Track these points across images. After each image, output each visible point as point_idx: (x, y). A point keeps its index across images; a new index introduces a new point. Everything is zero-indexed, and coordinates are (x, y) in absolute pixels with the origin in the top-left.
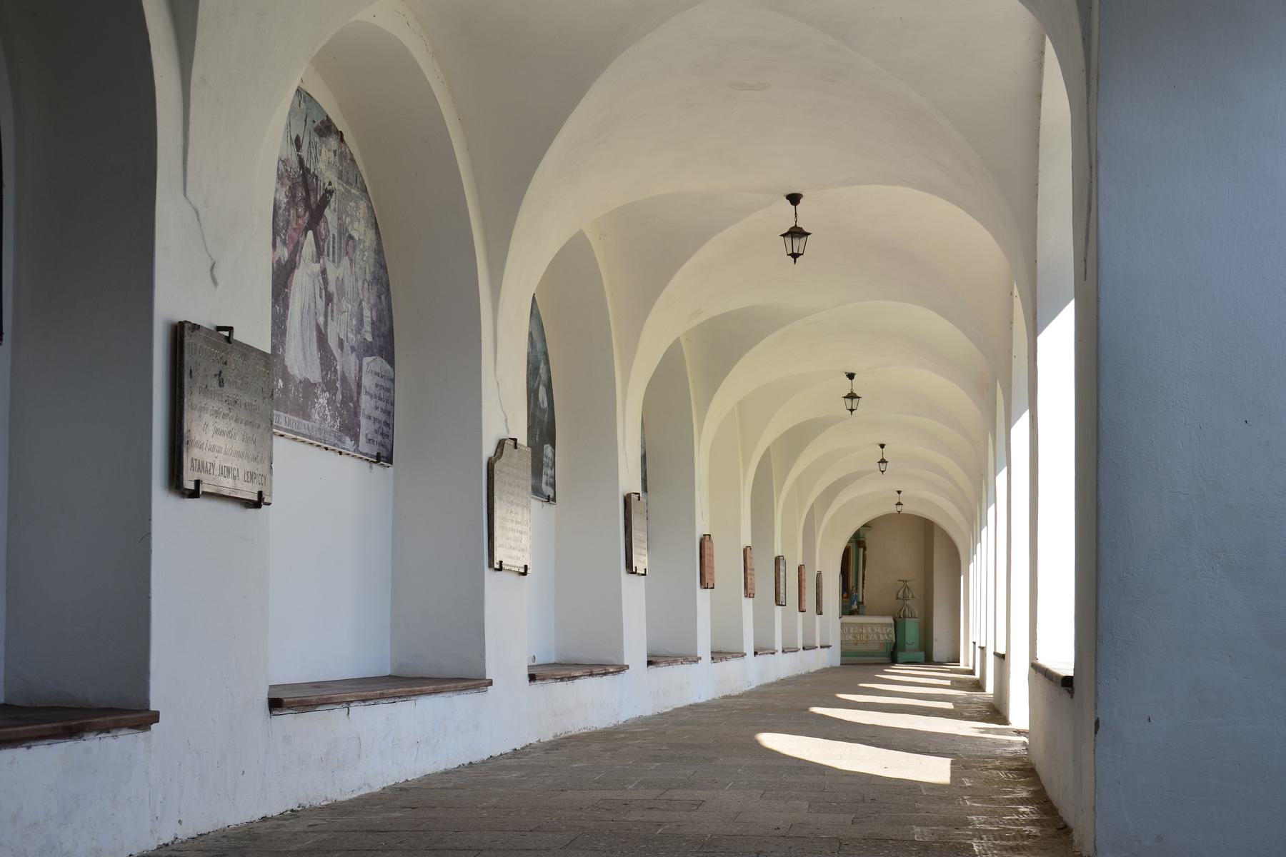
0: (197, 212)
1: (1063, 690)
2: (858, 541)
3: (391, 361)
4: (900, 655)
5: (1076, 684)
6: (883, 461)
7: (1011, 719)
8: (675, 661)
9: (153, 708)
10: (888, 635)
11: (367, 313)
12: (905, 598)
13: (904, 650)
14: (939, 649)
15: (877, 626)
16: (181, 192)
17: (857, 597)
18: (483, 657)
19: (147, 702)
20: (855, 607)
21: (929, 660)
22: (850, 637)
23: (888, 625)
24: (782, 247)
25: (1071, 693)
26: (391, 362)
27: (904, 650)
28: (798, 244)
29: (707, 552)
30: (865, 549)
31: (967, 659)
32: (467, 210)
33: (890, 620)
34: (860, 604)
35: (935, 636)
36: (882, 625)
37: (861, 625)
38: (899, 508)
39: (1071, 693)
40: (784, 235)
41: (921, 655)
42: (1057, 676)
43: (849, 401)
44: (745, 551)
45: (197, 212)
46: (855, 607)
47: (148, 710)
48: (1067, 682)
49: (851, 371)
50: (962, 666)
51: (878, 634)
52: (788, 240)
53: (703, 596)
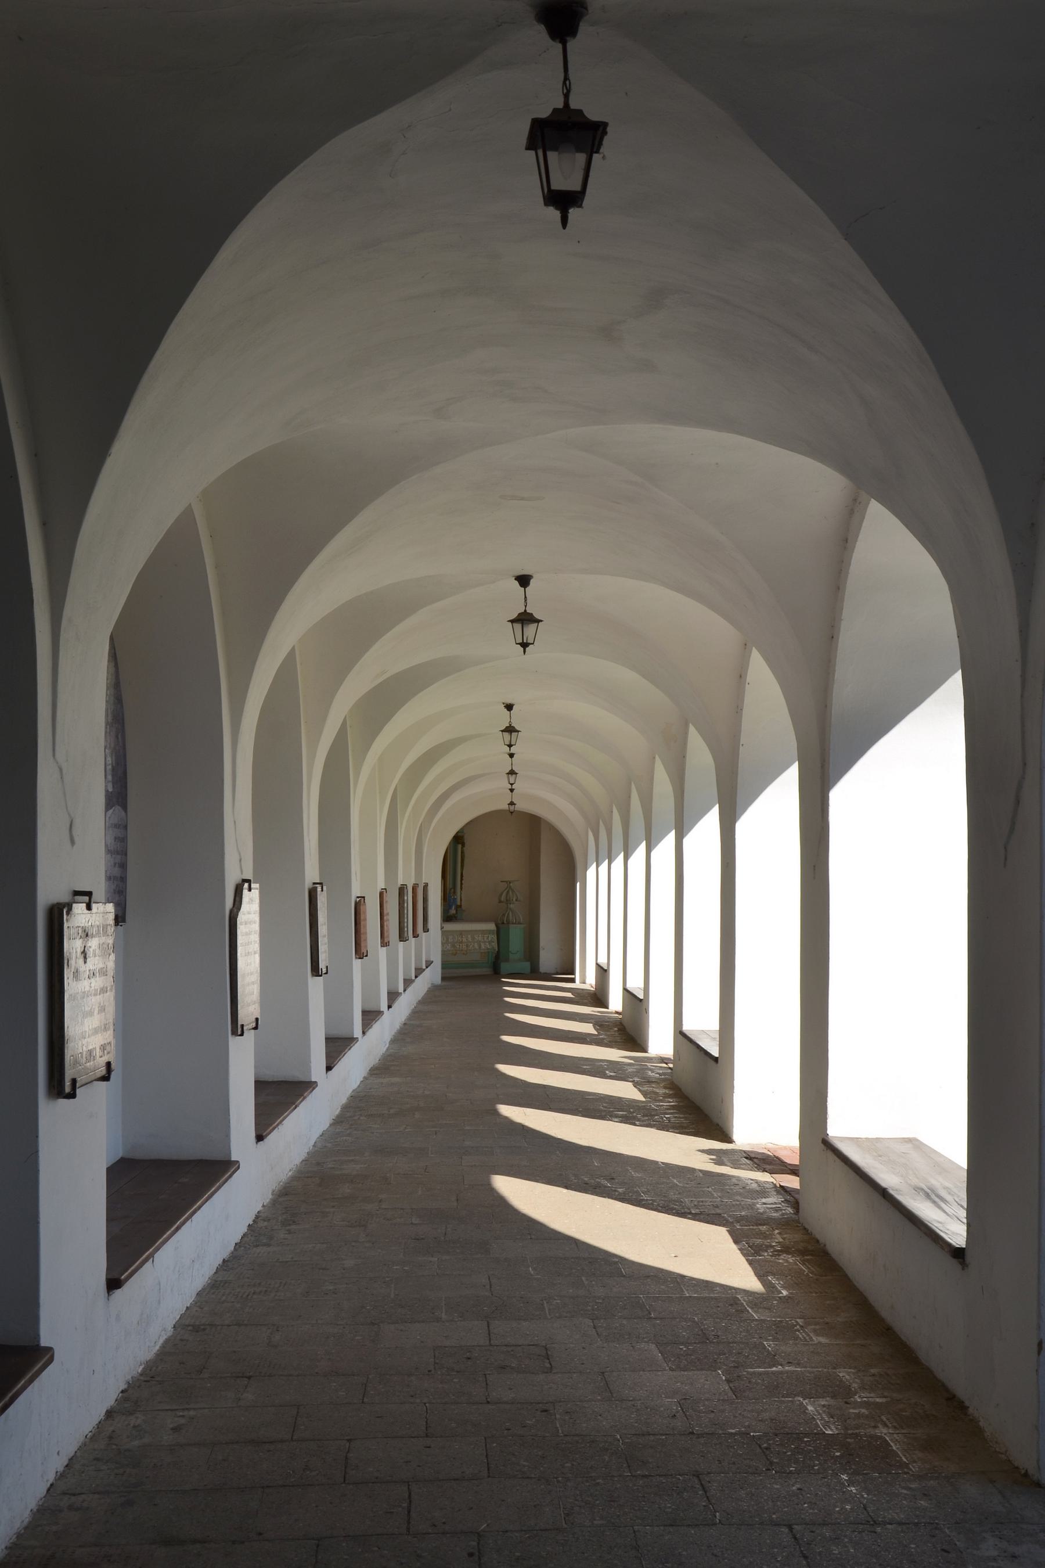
0: (61, 770)
1: (954, 1261)
2: (458, 839)
3: (125, 807)
4: (505, 967)
5: (969, 1258)
6: (512, 772)
7: (735, 1137)
8: (117, 872)
9: (44, 1343)
10: (490, 944)
11: (109, 759)
12: (508, 901)
13: (507, 960)
14: (547, 958)
15: (479, 933)
16: (51, 753)
17: (455, 899)
18: (228, 1136)
19: (37, 1336)
20: (453, 911)
21: (535, 973)
22: (449, 947)
23: (490, 932)
24: (508, 635)
25: (964, 1265)
26: (126, 811)
27: (507, 960)
28: (530, 630)
29: (386, 934)
30: (463, 845)
31: (586, 979)
32: (215, 635)
33: (492, 926)
34: (459, 907)
35: (542, 944)
36: (483, 932)
37: (461, 933)
38: (512, 808)
39: (964, 1265)
40: (512, 621)
41: (526, 966)
42: (949, 1245)
43: (506, 735)
44: (381, 894)
45: (61, 770)
46: (453, 911)
47: (38, 1345)
48: (958, 1253)
49: (509, 701)
50: (577, 985)
51: (479, 943)
52: (518, 626)
53: (357, 964)
